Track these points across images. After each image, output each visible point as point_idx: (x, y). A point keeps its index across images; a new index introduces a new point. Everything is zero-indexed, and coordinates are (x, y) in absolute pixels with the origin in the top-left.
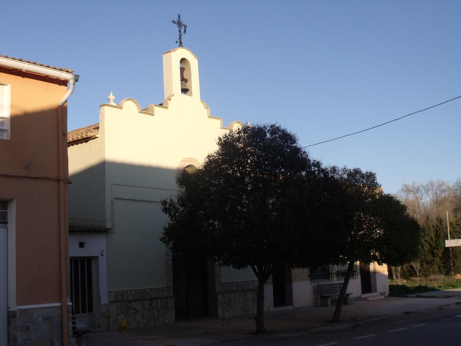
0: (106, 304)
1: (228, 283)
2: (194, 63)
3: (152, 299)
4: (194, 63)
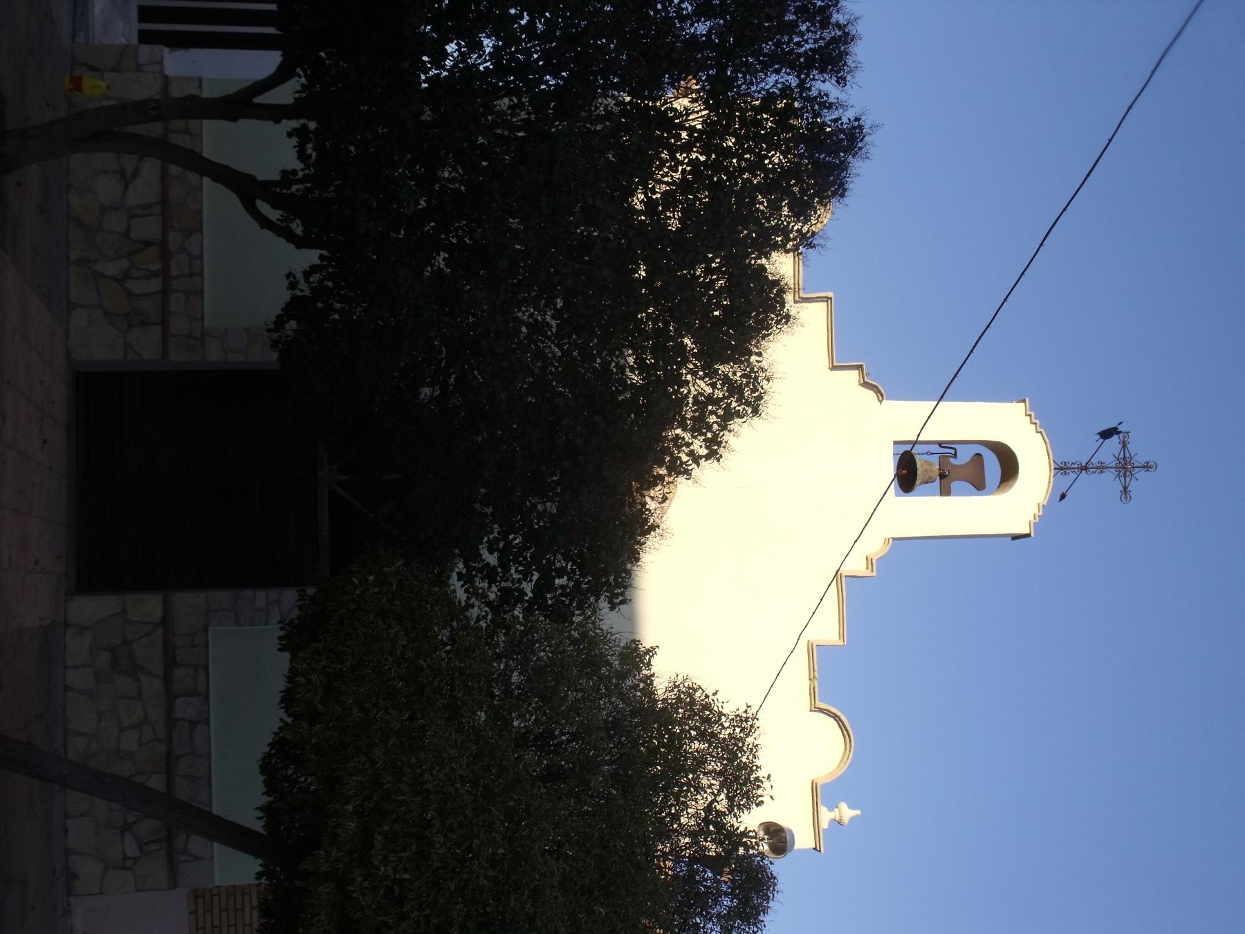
0: (161, 62)
1: (206, 667)
2: (1014, 509)
3: (165, 256)
4: (1014, 509)
